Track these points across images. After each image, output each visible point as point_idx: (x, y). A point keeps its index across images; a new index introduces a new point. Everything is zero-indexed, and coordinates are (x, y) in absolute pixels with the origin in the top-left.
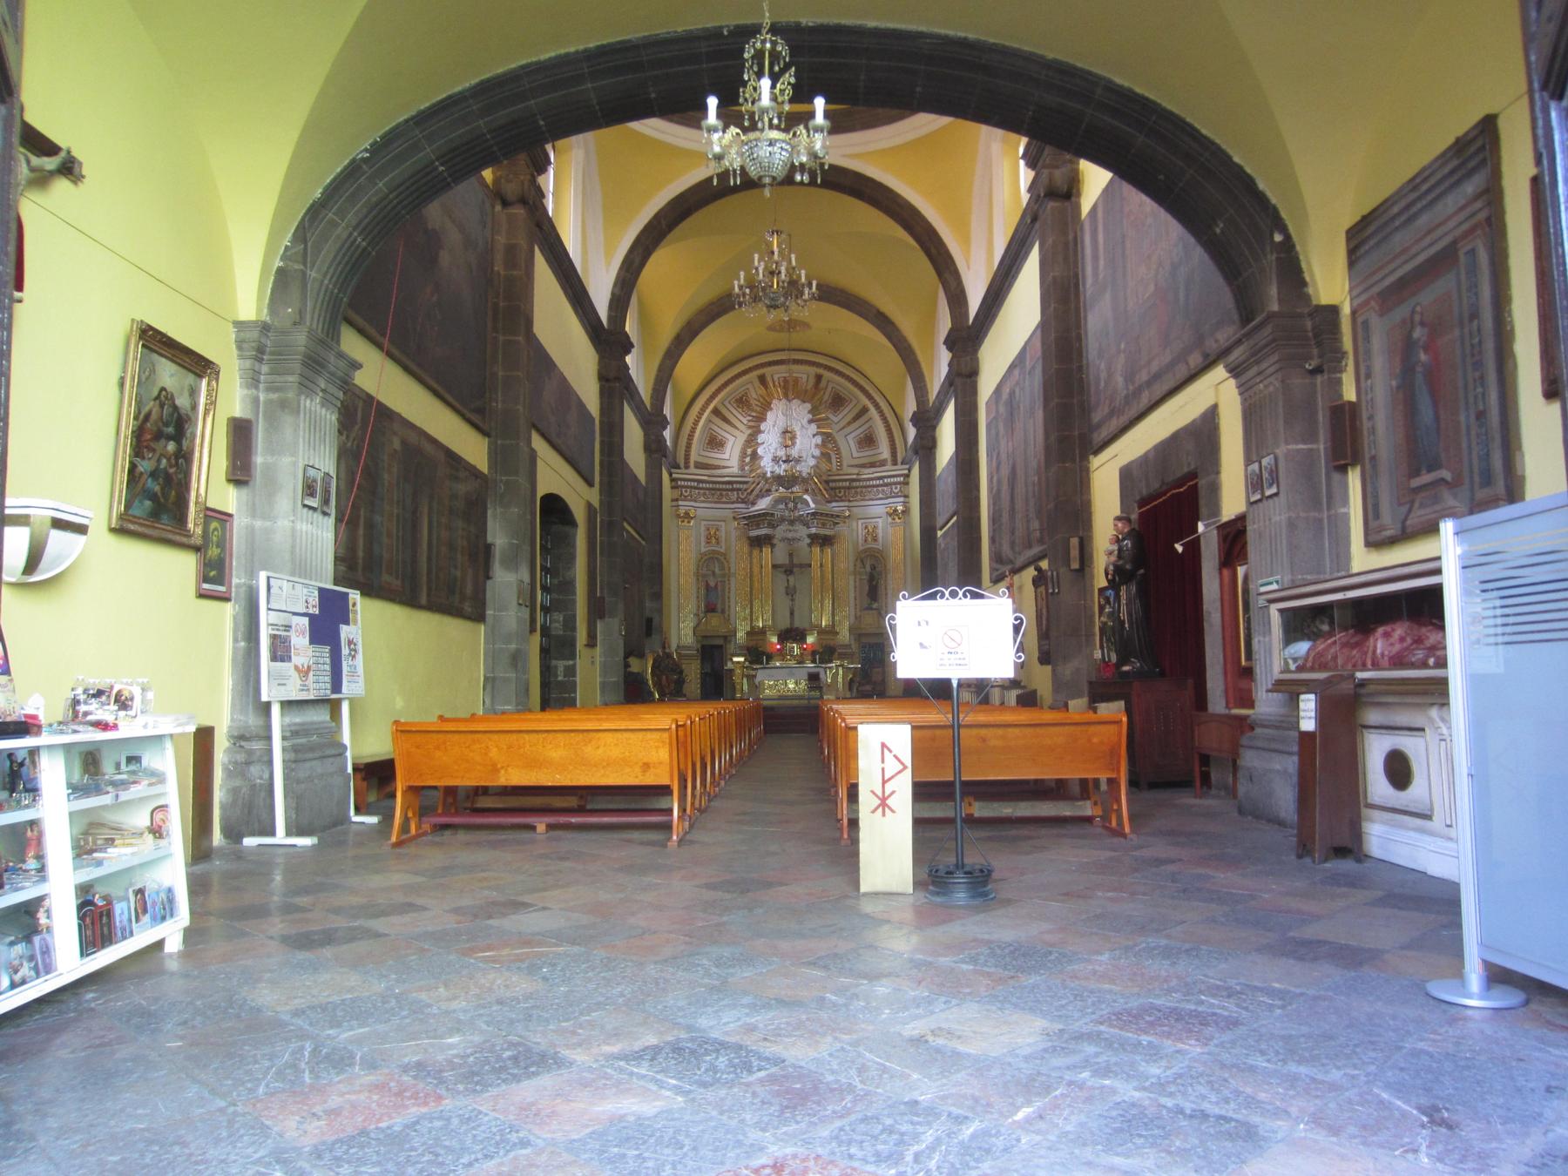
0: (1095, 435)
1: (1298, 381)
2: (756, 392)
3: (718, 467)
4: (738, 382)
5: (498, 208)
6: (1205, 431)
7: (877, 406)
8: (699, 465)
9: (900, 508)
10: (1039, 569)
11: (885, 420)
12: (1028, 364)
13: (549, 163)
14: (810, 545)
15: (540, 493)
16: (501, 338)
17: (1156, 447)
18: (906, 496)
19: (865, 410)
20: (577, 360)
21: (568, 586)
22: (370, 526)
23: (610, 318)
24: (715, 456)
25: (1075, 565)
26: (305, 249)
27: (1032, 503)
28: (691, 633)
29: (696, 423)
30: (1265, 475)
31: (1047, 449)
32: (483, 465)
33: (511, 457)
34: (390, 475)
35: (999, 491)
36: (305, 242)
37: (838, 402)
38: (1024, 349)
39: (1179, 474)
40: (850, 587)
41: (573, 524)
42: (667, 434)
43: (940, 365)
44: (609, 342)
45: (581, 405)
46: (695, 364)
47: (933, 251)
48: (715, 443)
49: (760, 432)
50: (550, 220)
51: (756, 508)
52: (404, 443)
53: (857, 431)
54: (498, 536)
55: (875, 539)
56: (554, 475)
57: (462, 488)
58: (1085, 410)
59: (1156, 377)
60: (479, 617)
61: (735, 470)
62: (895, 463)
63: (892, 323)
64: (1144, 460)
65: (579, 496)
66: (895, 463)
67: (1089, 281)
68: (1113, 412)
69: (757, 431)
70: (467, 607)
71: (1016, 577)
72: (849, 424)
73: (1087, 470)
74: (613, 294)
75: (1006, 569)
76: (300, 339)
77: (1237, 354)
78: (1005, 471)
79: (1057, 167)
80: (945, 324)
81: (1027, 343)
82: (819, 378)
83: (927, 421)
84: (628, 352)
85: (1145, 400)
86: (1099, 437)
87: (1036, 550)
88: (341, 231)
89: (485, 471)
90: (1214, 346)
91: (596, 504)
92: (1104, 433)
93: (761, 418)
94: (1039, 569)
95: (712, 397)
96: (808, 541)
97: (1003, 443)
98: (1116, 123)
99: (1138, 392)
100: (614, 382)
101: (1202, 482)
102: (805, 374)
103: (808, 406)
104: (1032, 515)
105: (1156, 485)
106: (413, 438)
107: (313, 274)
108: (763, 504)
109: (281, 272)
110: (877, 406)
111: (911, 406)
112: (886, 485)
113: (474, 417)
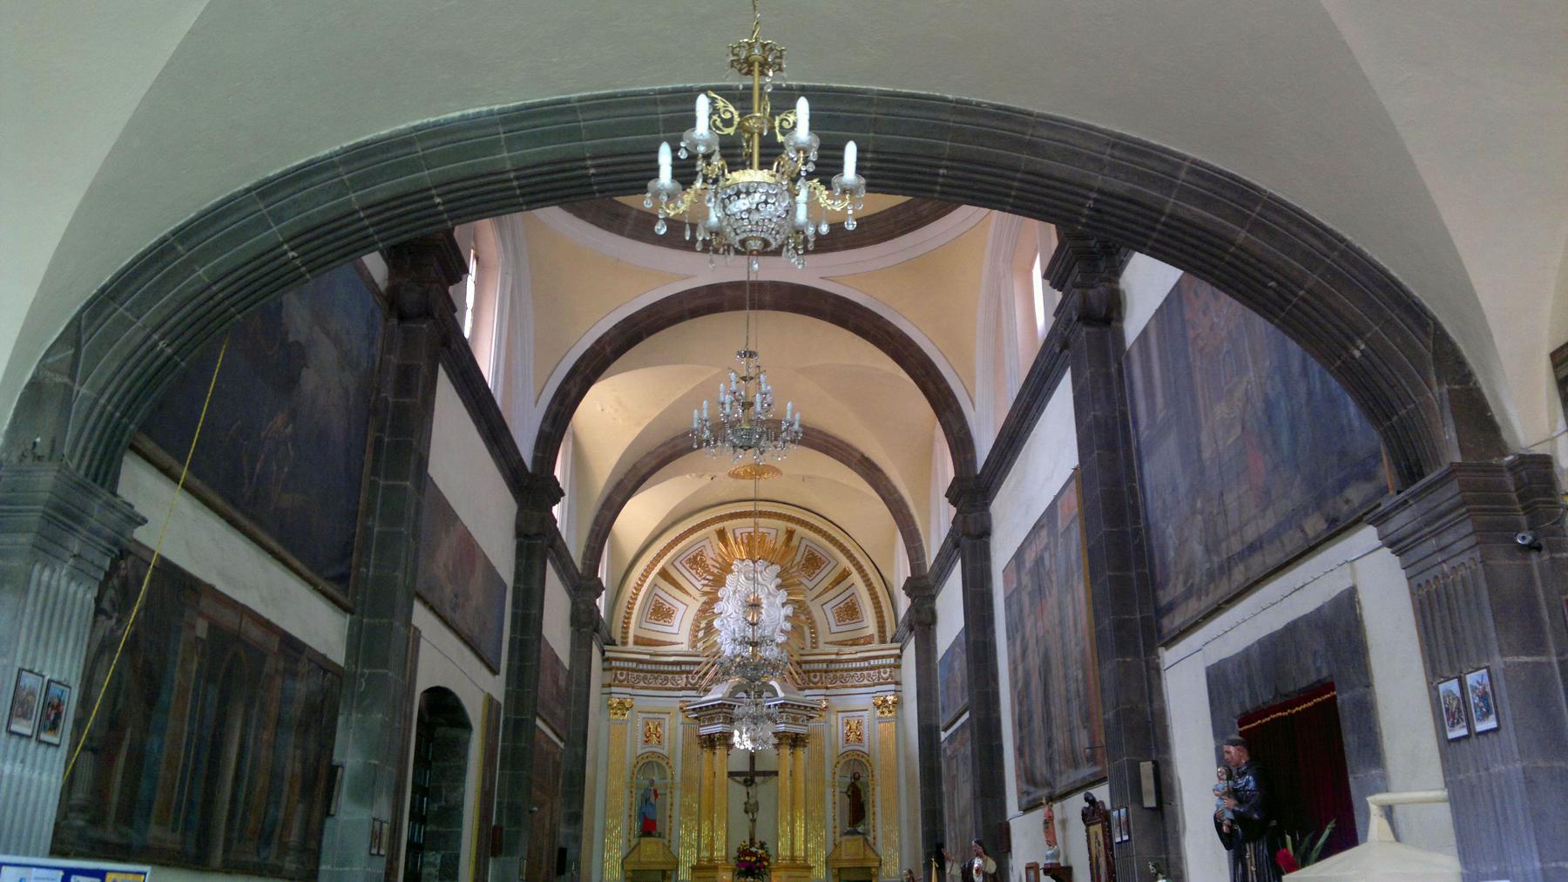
0: (1166, 622)
1: (1503, 562)
2: (713, 552)
4: (692, 538)
5: (395, 321)
6: (1341, 625)
7: (860, 568)
8: (639, 641)
9: (891, 698)
11: (870, 586)
12: (1061, 525)
13: (466, 271)
14: (777, 746)
15: (422, 684)
16: (382, 482)
17: (1260, 642)
19: (845, 575)
21: (452, 814)
22: (137, 758)
23: (535, 460)
24: (657, 630)
25: (1150, 802)
26: (76, 356)
27: (1075, 704)
28: (619, 868)
29: (638, 588)
30: (1473, 699)
31: (1099, 638)
32: (338, 655)
33: (384, 640)
34: (184, 671)
35: (1027, 684)
36: (78, 346)
37: (813, 562)
38: (1053, 506)
39: (1303, 683)
40: (833, 804)
41: (466, 725)
42: (601, 602)
43: (938, 520)
44: (533, 488)
45: (490, 568)
46: (639, 517)
47: (931, 386)
48: (661, 613)
49: (717, 599)
50: (464, 342)
51: (710, 697)
52: (214, 628)
53: (835, 599)
54: (349, 755)
56: (440, 659)
57: (301, 689)
58: (1151, 583)
59: (1252, 548)
62: (883, 641)
63: (879, 470)
65: (481, 690)
66: (883, 641)
68: (1189, 594)
69: (712, 600)
71: (1056, 807)
72: (826, 590)
73: (1158, 670)
76: (45, 479)
77: (1400, 522)
78: (1034, 661)
79: (1092, 287)
80: (946, 471)
81: (1056, 498)
82: (790, 534)
83: (923, 589)
84: (557, 501)
85: (1239, 576)
87: (1086, 771)
88: (135, 333)
90: (1345, 508)
91: (500, 697)
93: (719, 582)
94: (1091, 800)
97: (1029, 623)
98: (1208, 215)
99: (1226, 568)
100: (535, 539)
101: (1343, 697)
102: (773, 529)
103: (777, 568)
104: (1077, 720)
105: (1266, 697)
106: (228, 619)
107: (83, 390)
108: (717, 693)
109: (35, 386)
110: (860, 568)
111: (901, 571)
112: (872, 668)
113: (330, 589)
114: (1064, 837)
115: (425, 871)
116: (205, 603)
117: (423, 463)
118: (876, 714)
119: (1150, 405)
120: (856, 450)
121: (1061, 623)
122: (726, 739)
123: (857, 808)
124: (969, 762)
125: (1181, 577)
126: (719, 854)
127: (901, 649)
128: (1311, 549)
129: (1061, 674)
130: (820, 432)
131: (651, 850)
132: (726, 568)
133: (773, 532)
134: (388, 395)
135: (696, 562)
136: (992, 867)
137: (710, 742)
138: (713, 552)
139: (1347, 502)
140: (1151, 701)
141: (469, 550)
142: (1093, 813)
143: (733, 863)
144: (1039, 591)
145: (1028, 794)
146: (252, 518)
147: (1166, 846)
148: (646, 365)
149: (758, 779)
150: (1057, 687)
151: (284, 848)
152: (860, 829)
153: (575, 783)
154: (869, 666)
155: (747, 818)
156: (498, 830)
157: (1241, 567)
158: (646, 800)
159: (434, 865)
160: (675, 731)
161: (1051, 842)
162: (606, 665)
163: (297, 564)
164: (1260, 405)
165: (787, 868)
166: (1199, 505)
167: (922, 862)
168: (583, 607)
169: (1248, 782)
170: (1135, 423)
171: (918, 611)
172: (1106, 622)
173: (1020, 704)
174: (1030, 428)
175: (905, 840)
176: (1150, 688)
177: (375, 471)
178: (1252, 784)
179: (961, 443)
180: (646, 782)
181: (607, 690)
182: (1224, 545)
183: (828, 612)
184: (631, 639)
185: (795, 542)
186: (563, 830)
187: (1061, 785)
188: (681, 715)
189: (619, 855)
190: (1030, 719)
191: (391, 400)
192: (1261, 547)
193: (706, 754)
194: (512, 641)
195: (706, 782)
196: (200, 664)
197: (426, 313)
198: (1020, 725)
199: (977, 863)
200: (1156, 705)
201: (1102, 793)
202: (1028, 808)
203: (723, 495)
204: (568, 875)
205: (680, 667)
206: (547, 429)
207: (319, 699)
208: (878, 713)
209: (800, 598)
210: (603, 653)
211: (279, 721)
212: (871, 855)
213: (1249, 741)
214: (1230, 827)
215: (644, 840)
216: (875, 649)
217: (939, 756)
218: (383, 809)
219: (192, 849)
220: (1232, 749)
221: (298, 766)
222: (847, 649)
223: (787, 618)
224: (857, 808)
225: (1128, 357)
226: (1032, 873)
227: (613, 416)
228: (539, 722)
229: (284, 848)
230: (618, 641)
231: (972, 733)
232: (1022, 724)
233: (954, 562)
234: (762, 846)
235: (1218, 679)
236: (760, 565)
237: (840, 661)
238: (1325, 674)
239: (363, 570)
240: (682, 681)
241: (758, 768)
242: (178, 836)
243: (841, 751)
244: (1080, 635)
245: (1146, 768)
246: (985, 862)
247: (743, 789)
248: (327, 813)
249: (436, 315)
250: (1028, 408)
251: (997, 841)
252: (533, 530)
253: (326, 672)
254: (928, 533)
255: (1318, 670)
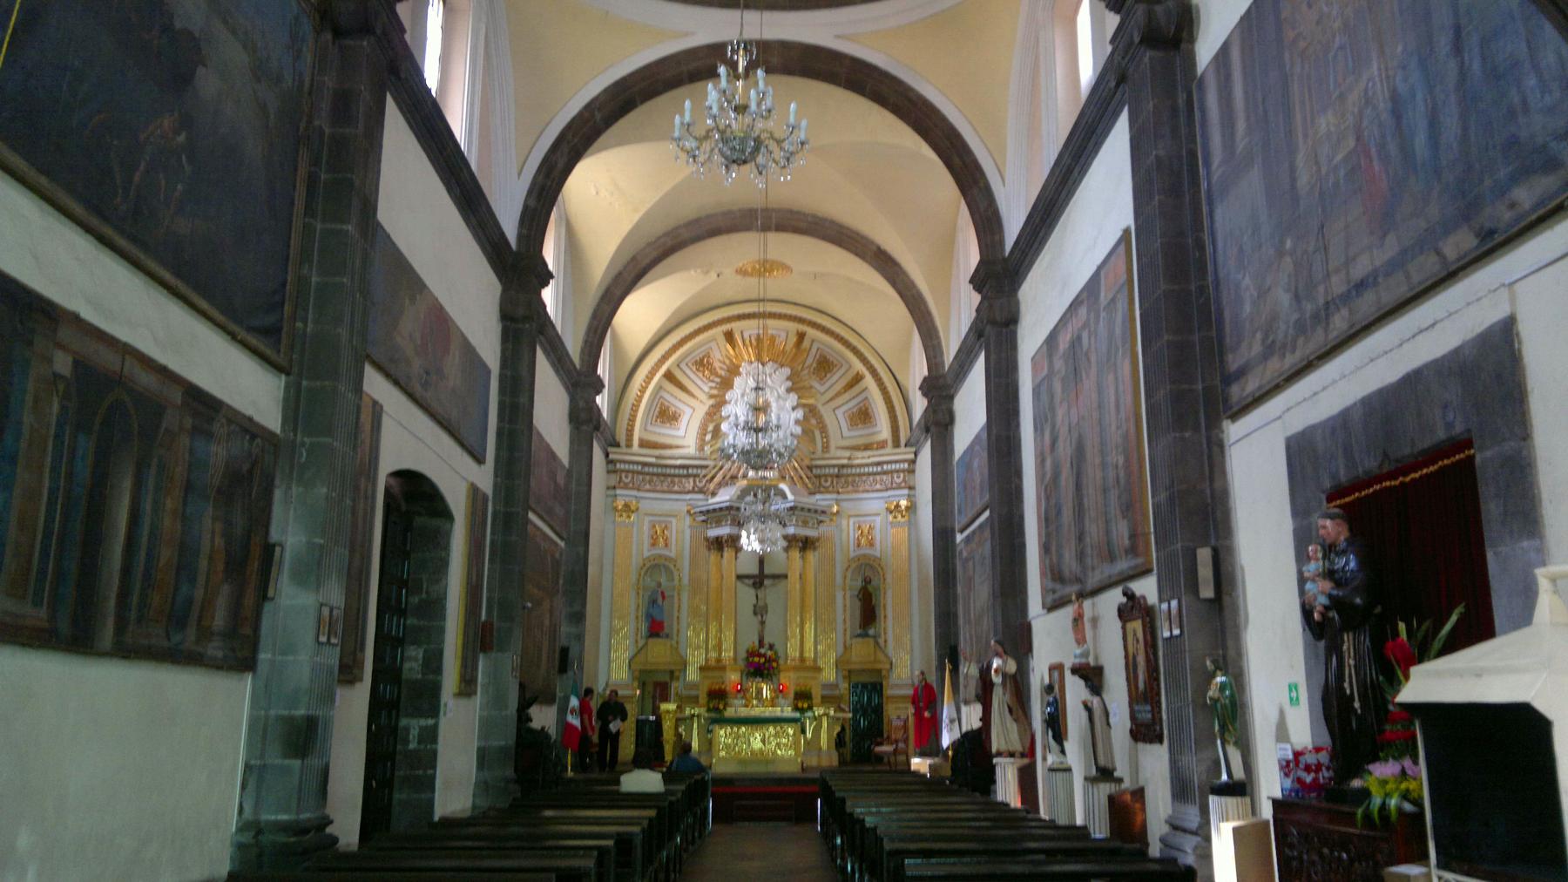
2: (720, 353)
3: (678, 447)
5: (329, 36)
8: (644, 444)
9: (903, 503)
10: (1129, 595)
12: (1104, 298)
14: (787, 549)
15: (388, 463)
16: (319, 226)
18: (911, 488)
19: (858, 378)
20: (467, 293)
23: (520, 237)
24: (663, 433)
25: (1207, 592)
27: (1113, 495)
28: (625, 668)
29: (643, 390)
32: (271, 417)
37: (825, 366)
39: (1426, 443)
40: (844, 608)
41: (447, 515)
42: (602, 401)
43: (959, 311)
45: (469, 350)
46: (640, 315)
47: (957, 161)
48: (667, 416)
51: (717, 499)
53: (848, 404)
54: (290, 531)
55: (871, 544)
56: (408, 439)
57: (219, 452)
58: (1216, 349)
59: (1361, 286)
60: (243, 661)
61: (691, 450)
64: (1341, 423)
65: (459, 476)
66: (896, 444)
67: (1216, 160)
68: (1269, 351)
69: (720, 403)
70: (214, 649)
71: (1087, 604)
72: (838, 394)
74: (526, 208)
75: (1072, 590)
78: (1065, 450)
80: (970, 255)
81: (1100, 268)
83: (940, 389)
84: (547, 284)
85: (1340, 323)
86: (1237, 392)
87: (1123, 565)
89: (278, 431)
90: (1508, 216)
92: (1251, 385)
93: (726, 384)
94: (1129, 595)
95: (664, 358)
96: (785, 544)
100: (523, 324)
102: (783, 332)
103: (786, 371)
105: (1370, 464)
108: (725, 496)
111: (917, 369)
112: (885, 473)
114: (1095, 637)
115: (407, 666)
116: (65, 333)
117: (369, 207)
118: (889, 518)
119: (1225, 129)
120: (872, 243)
121: (1100, 407)
122: (734, 541)
123: (868, 611)
124: (988, 561)
125: (1259, 336)
126: (728, 654)
127: (916, 454)
128: (1450, 276)
129: (1097, 461)
130: (833, 222)
131: (659, 652)
132: (734, 371)
133: (783, 335)
134: (323, 122)
135: (703, 364)
136: (1012, 667)
137: (718, 544)
138: (720, 353)
139: (1512, 206)
140: (1212, 480)
141: (440, 323)
142: (1133, 609)
143: (741, 664)
144: (1075, 374)
145: (1054, 592)
146: (133, 239)
147: (1224, 640)
148: (641, 139)
149: (766, 582)
150: (1093, 475)
151: (205, 634)
152: (871, 632)
153: (576, 582)
154: (881, 471)
155: (756, 620)
156: (487, 629)
157: (1345, 312)
158: (654, 602)
159: (416, 660)
160: (682, 536)
161: (1080, 640)
162: (611, 467)
163: (204, 305)
164: (1383, 105)
165: (795, 669)
166: (1289, 244)
167: (934, 663)
168: (581, 404)
169: (1347, 563)
170: (1207, 164)
171: (935, 412)
172: (1161, 394)
173: (1048, 498)
174: (1070, 194)
175: (917, 643)
176: (1211, 467)
177: (309, 210)
178: (1352, 565)
179: (987, 221)
180: (653, 584)
181: (611, 492)
182: (1321, 289)
183: (840, 416)
184: (636, 442)
185: (806, 344)
186: (565, 629)
187: (1093, 580)
188: (688, 521)
189: (627, 655)
190: (1059, 513)
191: (327, 131)
192: (1376, 283)
193: (713, 557)
194: (499, 433)
195: (713, 584)
196: (63, 408)
197: (366, 29)
198: (1047, 520)
199: (996, 663)
200: (1217, 485)
201: (1147, 588)
202: (1052, 607)
203: (730, 295)
204: (570, 673)
205: (687, 471)
206: (532, 203)
207: (246, 467)
208: (891, 518)
209: (811, 401)
210: (607, 455)
211: (189, 487)
212: (880, 656)
213: (1353, 516)
214: (1322, 614)
215: (652, 641)
216: (888, 454)
217: (954, 557)
218: (335, 595)
219: (64, 626)
220: (1328, 523)
221: (219, 541)
222: (859, 454)
223: (797, 422)
224: (868, 611)
225: (1201, 82)
226: (1056, 674)
227: (609, 196)
228: (531, 516)
229: (205, 634)
230: (623, 443)
231: (993, 534)
232: (1049, 520)
233: (977, 356)
234: (771, 647)
235: (1301, 452)
236: (769, 368)
237: (852, 466)
238: (1459, 428)
239: (299, 325)
240: (689, 484)
241: (767, 571)
242: (43, 613)
243: (852, 555)
244: (1122, 415)
245: (1204, 555)
246: (1005, 662)
247: (752, 591)
248: (263, 596)
249: (378, 32)
250: (1070, 171)
251: (1018, 641)
252: (521, 312)
253: (253, 437)
254: (947, 337)
255: (1449, 426)
